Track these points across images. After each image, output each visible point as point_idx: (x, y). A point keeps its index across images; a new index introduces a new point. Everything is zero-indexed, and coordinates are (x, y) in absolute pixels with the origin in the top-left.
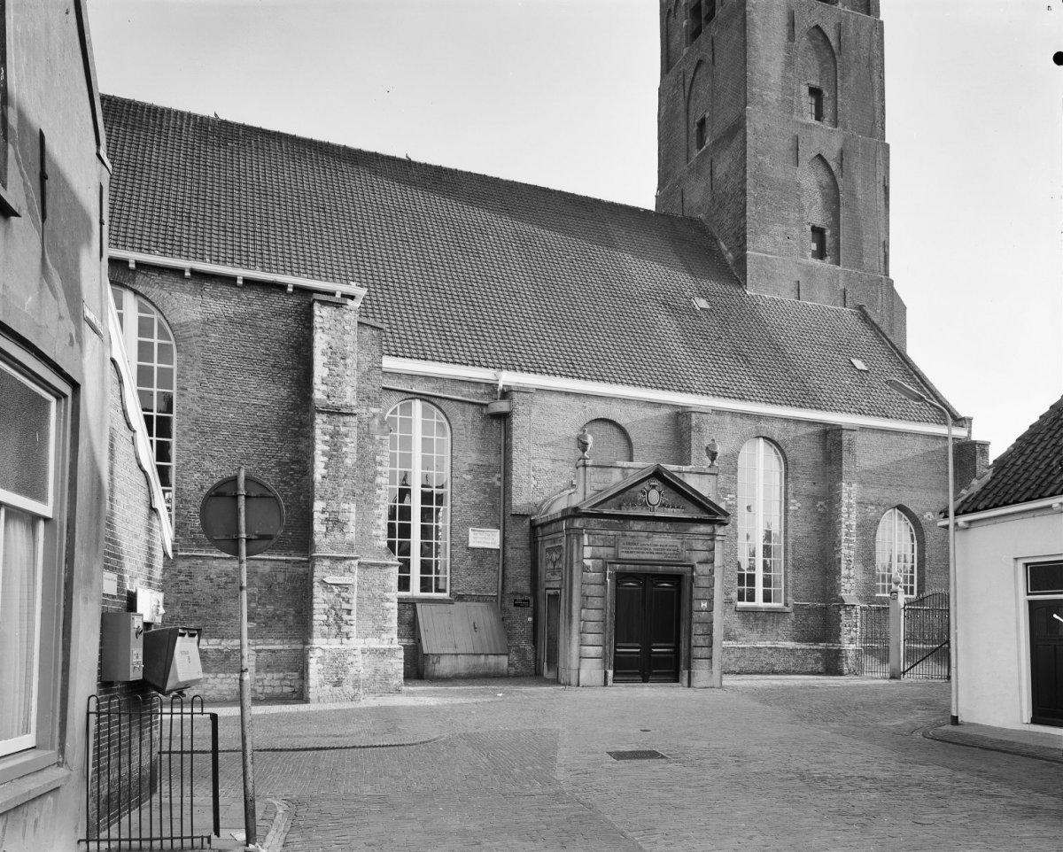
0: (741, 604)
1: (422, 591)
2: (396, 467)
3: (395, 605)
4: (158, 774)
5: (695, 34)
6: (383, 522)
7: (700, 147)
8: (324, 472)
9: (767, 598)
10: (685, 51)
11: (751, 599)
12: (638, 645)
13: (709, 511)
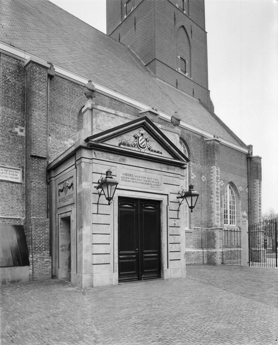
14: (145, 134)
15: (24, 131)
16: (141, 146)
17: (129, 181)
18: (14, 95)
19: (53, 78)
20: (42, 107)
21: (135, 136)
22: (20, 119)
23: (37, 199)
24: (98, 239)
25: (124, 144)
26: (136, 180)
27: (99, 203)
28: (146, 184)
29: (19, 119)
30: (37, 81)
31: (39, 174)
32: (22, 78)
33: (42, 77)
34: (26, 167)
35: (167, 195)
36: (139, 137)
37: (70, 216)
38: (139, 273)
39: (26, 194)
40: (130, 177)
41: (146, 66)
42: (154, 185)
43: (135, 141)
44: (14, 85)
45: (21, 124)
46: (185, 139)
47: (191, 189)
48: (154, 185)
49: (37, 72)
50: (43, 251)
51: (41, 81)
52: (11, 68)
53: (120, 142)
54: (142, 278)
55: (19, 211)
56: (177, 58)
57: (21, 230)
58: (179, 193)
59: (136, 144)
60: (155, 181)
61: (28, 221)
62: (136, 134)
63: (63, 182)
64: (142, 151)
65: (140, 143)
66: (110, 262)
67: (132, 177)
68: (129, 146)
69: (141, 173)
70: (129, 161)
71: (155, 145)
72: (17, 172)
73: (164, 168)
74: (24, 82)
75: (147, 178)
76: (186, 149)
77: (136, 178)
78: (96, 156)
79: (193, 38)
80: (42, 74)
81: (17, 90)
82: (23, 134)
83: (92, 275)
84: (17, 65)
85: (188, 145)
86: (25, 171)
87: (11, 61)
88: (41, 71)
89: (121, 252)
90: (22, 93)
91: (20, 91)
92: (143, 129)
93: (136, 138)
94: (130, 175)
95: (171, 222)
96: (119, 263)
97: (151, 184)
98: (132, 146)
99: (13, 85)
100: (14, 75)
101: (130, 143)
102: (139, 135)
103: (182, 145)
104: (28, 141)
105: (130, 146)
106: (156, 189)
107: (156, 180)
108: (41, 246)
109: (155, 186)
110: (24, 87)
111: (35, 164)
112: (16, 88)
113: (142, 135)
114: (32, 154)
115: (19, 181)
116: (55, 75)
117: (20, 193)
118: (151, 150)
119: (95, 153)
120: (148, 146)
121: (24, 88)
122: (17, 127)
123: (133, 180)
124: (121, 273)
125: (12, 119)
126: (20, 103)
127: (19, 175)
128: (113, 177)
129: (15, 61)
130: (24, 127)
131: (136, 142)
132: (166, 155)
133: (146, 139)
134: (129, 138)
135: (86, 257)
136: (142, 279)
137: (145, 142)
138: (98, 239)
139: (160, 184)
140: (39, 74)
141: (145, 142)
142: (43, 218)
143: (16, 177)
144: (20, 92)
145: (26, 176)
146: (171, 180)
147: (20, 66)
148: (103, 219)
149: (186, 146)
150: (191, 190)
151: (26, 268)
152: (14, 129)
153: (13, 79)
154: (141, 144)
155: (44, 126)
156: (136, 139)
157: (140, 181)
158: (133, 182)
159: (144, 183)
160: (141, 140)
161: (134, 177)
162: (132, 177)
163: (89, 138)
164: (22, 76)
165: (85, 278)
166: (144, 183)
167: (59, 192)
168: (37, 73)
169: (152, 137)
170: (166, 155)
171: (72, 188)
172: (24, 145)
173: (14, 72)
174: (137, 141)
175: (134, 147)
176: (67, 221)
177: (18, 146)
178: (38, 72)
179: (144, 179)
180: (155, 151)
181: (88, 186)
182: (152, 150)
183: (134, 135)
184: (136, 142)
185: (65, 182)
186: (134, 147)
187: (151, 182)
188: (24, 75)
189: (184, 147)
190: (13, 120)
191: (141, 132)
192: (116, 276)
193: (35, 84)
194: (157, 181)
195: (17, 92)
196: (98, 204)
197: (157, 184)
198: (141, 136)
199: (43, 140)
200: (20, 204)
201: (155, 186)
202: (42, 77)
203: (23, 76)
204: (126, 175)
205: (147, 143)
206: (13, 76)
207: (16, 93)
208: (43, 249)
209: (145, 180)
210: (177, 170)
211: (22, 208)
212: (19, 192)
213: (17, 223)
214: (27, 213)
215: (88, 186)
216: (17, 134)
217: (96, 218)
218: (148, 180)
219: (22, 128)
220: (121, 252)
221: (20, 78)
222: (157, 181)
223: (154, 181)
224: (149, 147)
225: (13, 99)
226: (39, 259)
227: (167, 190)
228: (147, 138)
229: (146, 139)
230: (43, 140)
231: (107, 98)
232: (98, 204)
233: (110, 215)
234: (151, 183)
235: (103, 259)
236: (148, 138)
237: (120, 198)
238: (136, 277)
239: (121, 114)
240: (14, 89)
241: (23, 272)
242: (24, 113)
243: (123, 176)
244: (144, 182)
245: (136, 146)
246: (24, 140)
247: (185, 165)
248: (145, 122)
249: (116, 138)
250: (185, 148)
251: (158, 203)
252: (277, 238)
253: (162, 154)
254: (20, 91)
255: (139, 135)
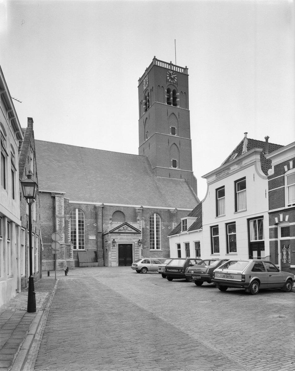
0: (151, 250)
1: (79, 249)
2: (74, 220)
3: (73, 252)
4: (172, 273)
5: (146, 110)
6: (70, 234)
7: (147, 138)
8: (59, 228)
9: (157, 248)
10: (144, 113)
11: (154, 248)
13: (137, 231)
23: (100, 244)
24: (113, 255)
25: (120, 230)
39: (97, 242)
56: (170, 161)
57: (96, 252)
61: (97, 250)
69: (126, 237)
70: (121, 234)
71: (129, 229)
73: (133, 235)
79: (181, 147)
82: (96, 225)
83: (111, 264)
95: (136, 250)
101: (122, 229)
104: (97, 228)
111: (99, 234)
115: (95, 239)
127: (95, 237)
132: (134, 231)
134: (122, 228)
135: (110, 259)
138: (113, 255)
142: (101, 249)
145: (97, 238)
146: (136, 238)
148: (114, 250)
151: (97, 263)
165: (110, 265)
170: (134, 231)
176: (107, 250)
181: (110, 242)
192: (118, 264)
210: (139, 235)
211: (96, 246)
212: (95, 242)
213: (95, 251)
214: (97, 248)
215: (110, 242)
217: (112, 250)
226: (101, 260)
227: (134, 241)
231: (122, 207)
233: (117, 248)
235: (114, 260)
239: (119, 222)
241: (97, 264)
251: (131, 245)
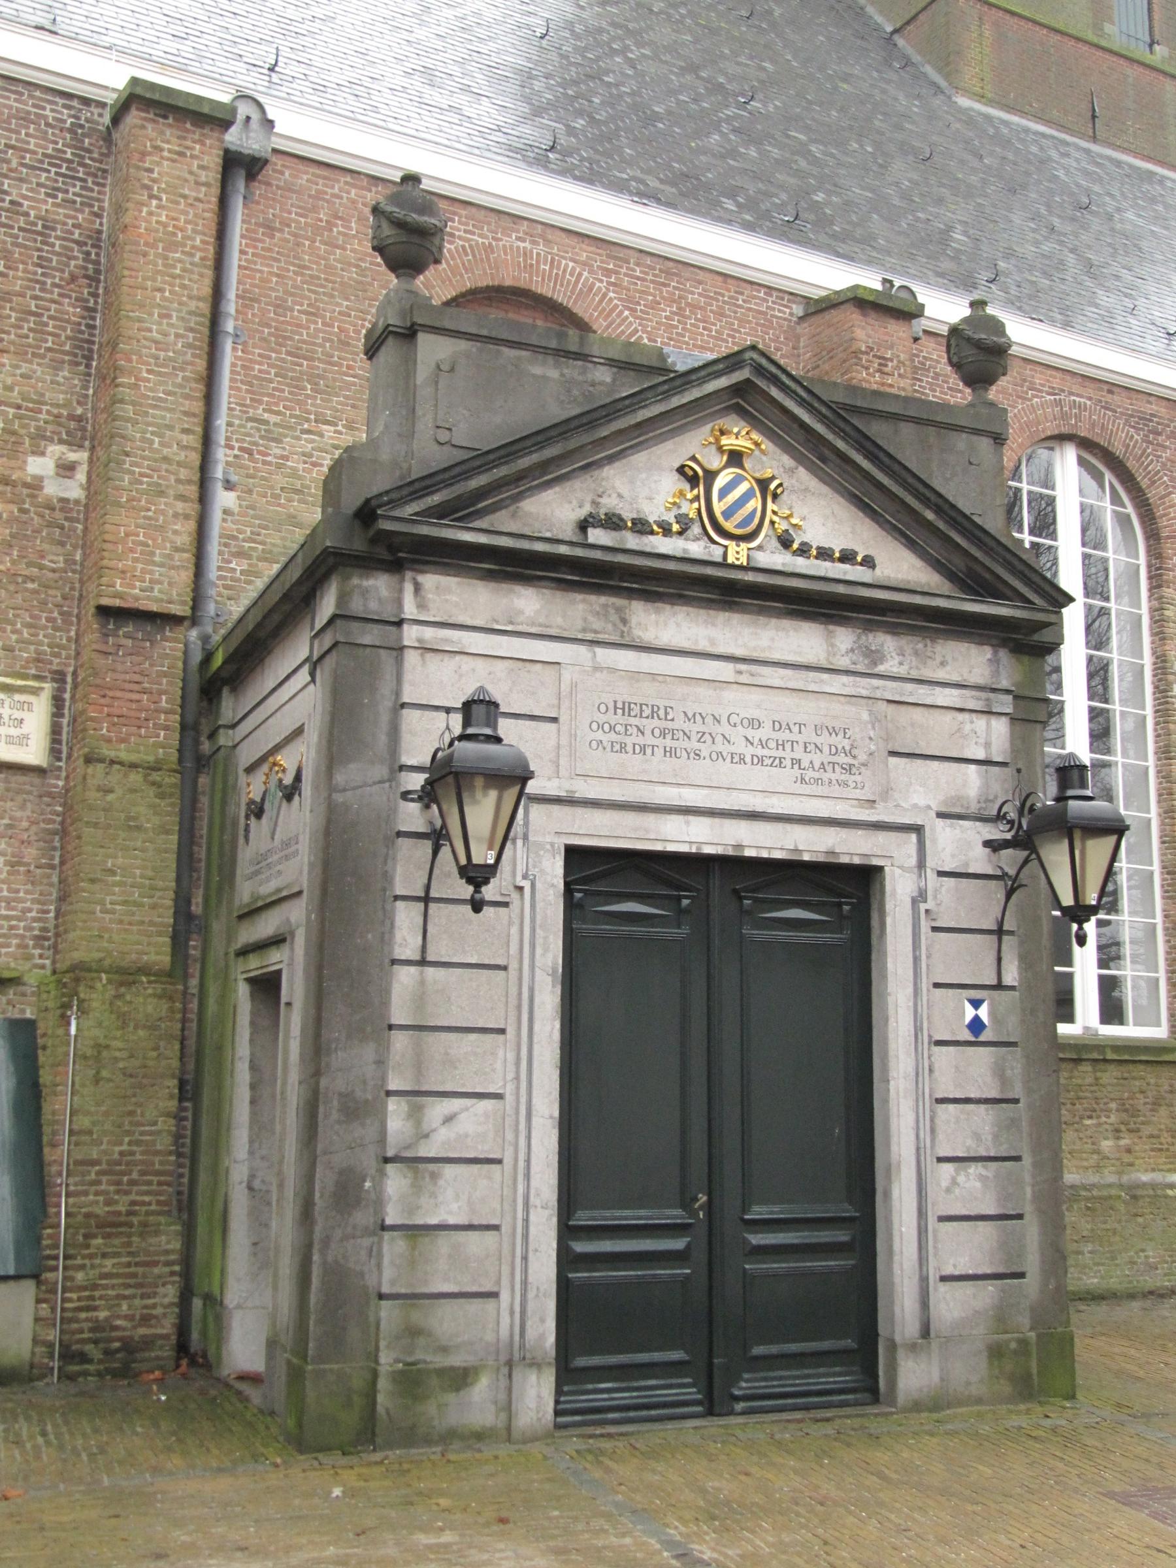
12: (675, 1215)
14: (757, 452)
15: (81, 476)
16: (729, 526)
17: (643, 749)
18: (37, 282)
19: (268, 171)
20: (177, 336)
21: (683, 466)
22: (64, 406)
26: (694, 737)
27: (433, 894)
28: (761, 760)
29: (58, 406)
30: (160, 199)
31: (137, 714)
32: (92, 190)
33: (191, 173)
34: (75, 673)
35: (918, 829)
36: (711, 475)
37: (279, 973)
38: (710, 1365)
40: (648, 724)
41: (896, 37)
42: (817, 765)
43: (689, 496)
44: (44, 226)
45: (68, 433)
46: (1118, 450)
47: (1073, 788)
48: (817, 765)
49: (162, 150)
50: (133, 1183)
51: (185, 197)
52: (32, 141)
53: (587, 509)
54: (737, 1399)
55: (17, 936)
58: (1000, 817)
59: (692, 514)
60: (824, 739)
62: (693, 458)
63: (263, 759)
64: (731, 559)
65: (718, 508)
66: (498, 1282)
67: (664, 724)
68: (641, 532)
72: (22, 706)
74: (101, 208)
75: (768, 725)
76: (1130, 510)
77: (687, 726)
78: (421, 606)
80: (192, 157)
81: (58, 254)
82: (74, 490)
84: (68, 125)
85: (1144, 483)
86: (67, 696)
87: (34, 106)
88: (189, 143)
89: (588, 1213)
90: (86, 269)
91: (75, 258)
92: (743, 423)
93: (693, 480)
94: (647, 712)
96: (564, 1287)
97: (796, 762)
98: (666, 531)
99: (39, 228)
100: (44, 175)
101: (654, 512)
102: (715, 461)
103: (1104, 491)
105: (652, 533)
106: (836, 791)
107: (833, 731)
108: (121, 1153)
109: (825, 777)
110: (100, 232)
112: (53, 245)
113: (735, 458)
114: (105, 601)
116: (275, 151)
117: (34, 828)
118: (795, 546)
119: (418, 588)
120: (772, 523)
121: (99, 240)
122: (43, 454)
123: (668, 742)
124: (581, 1362)
125: (19, 407)
126: (68, 321)
128: (505, 728)
129: (56, 103)
130: (81, 446)
131: (692, 501)
132: (899, 567)
133: (763, 484)
136: (740, 1406)
137: (755, 503)
139: (862, 757)
140: (173, 161)
141: (755, 503)
143: (14, 732)
144: (73, 263)
147: (82, 126)
149: (1128, 490)
150: (1070, 793)
152: (22, 468)
153: (42, 196)
154: (728, 514)
155: (184, 437)
156: (692, 489)
157: (720, 746)
158: (670, 752)
159: (748, 759)
160: (731, 491)
161: (680, 723)
162: (664, 724)
163: (374, 503)
164: (90, 180)
166: (748, 759)
167: (247, 817)
168: (166, 154)
169: (801, 470)
170: (899, 567)
171: (296, 798)
172: (75, 547)
173: (50, 164)
174: (697, 498)
175: (680, 533)
177: (43, 557)
178: (170, 151)
179: (750, 733)
180: (824, 554)
182: (803, 544)
183: (677, 465)
184: (696, 505)
185: (271, 759)
186: (680, 533)
187: (799, 748)
188: (105, 171)
189: (1116, 499)
190: (20, 417)
191: (727, 442)
193: (151, 213)
194: (840, 741)
195: (58, 262)
196: (426, 899)
197: (842, 759)
198: (725, 467)
199: (176, 515)
200: (27, 892)
201: (825, 777)
202: (191, 173)
203: (95, 176)
204: (626, 708)
205: (770, 506)
206: (38, 185)
207: (53, 269)
208: (135, 1176)
209: (756, 735)
216: (41, 488)
218: (785, 735)
219: (73, 456)
220: (582, 1218)
221: (77, 190)
222: (840, 741)
223: (819, 740)
224: (782, 526)
225: (33, 303)
228: (768, 473)
229: (763, 484)
230: (176, 515)
232: (426, 899)
234: (799, 753)
236: (773, 478)
237: (576, 856)
238: (692, 1393)
240: (39, 250)
242: (89, 375)
243: (602, 718)
244: (748, 751)
245: (696, 529)
246: (78, 521)
247: (1045, 631)
248: (748, 381)
249: (557, 489)
250: (1123, 506)
252: (590, 1386)
253: (873, 567)
254: (75, 258)
255: (715, 461)
